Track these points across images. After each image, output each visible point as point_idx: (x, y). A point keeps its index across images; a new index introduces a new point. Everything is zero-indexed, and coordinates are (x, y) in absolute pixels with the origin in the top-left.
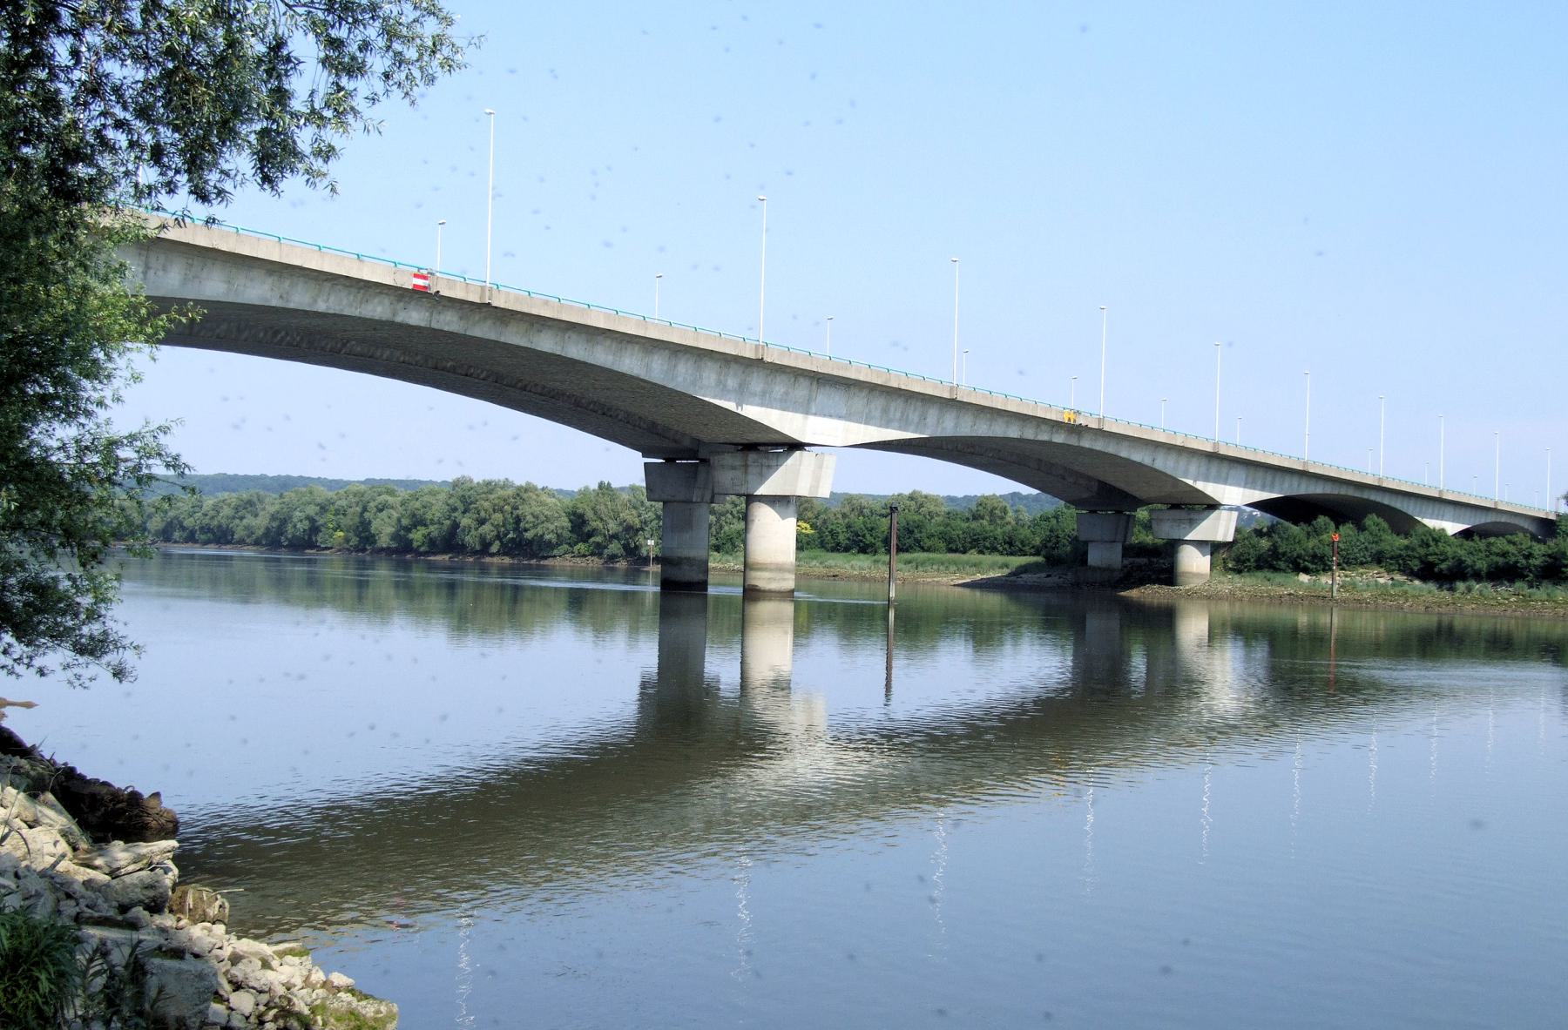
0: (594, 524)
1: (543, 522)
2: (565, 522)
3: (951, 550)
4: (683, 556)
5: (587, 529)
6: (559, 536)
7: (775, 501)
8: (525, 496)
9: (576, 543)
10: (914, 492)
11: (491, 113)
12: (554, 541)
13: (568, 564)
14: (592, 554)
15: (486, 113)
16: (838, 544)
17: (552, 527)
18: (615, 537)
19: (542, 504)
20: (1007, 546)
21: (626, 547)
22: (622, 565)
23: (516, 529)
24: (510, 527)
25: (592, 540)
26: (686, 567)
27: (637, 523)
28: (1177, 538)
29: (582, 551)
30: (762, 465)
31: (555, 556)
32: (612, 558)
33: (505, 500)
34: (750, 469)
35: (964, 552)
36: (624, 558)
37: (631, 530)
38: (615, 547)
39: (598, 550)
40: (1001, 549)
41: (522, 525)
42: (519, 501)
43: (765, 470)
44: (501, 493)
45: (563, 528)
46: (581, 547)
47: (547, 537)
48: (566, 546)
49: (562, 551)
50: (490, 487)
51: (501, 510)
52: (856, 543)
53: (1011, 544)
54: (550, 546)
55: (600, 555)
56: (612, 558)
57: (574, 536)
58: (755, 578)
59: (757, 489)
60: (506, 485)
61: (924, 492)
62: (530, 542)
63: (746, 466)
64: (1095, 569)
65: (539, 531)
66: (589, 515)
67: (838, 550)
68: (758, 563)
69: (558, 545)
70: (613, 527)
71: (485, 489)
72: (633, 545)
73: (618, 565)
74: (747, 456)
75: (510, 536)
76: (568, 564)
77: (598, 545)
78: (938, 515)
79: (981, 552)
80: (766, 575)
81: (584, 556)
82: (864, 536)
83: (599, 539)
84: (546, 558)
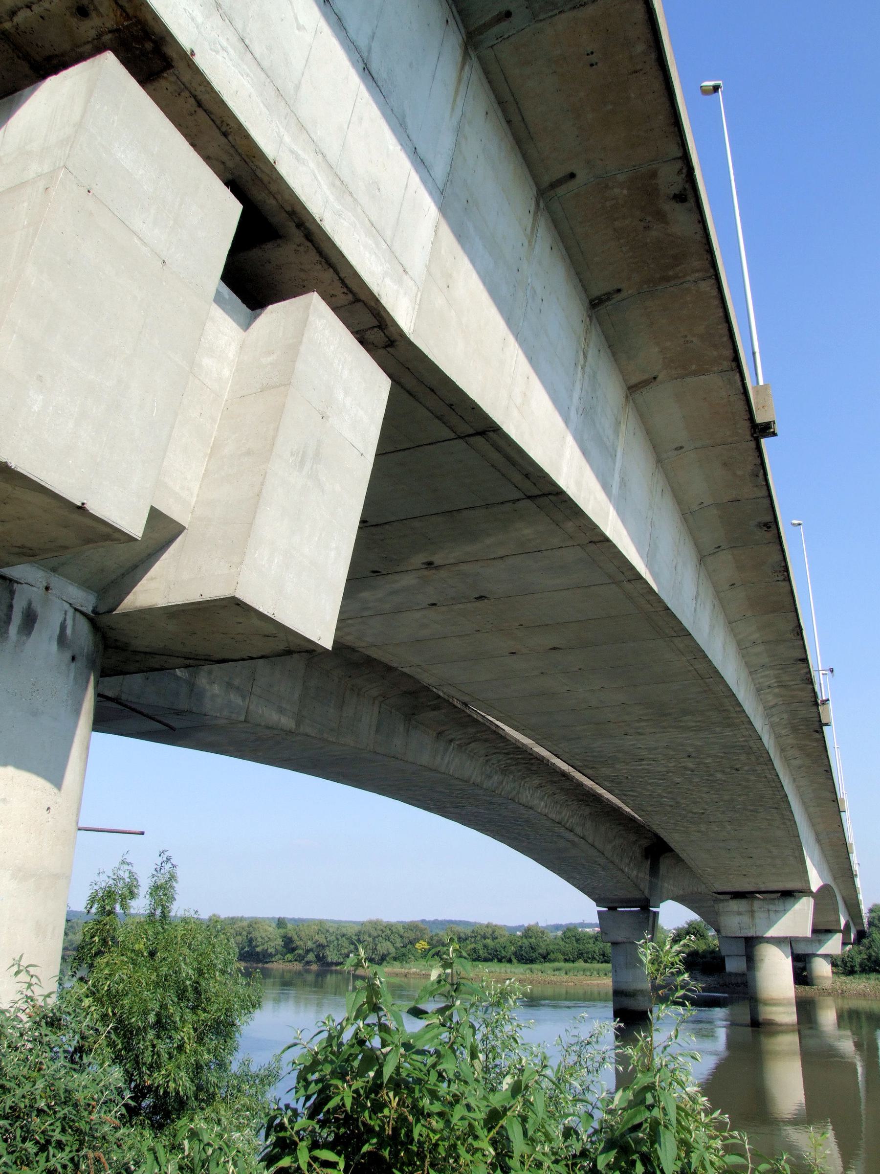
0: (298, 943)
1: (267, 942)
2: (280, 942)
3: (566, 960)
4: (638, 989)
5: (294, 945)
6: (276, 949)
7: (778, 941)
8: (256, 926)
9: (286, 954)
10: (489, 923)
11: (799, 524)
12: (273, 953)
13: (281, 966)
14: (296, 960)
15: (794, 525)
16: (479, 956)
17: (273, 945)
18: (311, 950)
19: (266, 931)
20: (601, 957)
21: (317, 956)
22: (314, 967)
23: (249, 946)
24: (246, 944)
25: (296, 952)
26: (640, 998)
27: (324, 942)
28: (810, 952)
29: (289, 959)
30: (769, 910)
31: (273, 962)
32: (308, 963)
33: (243, 928)
34: (756, 914)
35: (573, 961)
36: (315, 962)
37: (322, 947)
38: (311, 957)
39: (300, 959)
40: (598, 958)
41: (254, 943)
42: (251, 929)
43: (772, 914)
44: (240, 924)
45: (279, 945)
46: (289, 956)
47: (270, 951)
48: (280, 956)
49: (277, 959)
50: (233, 921)
51: (240, 934)
52: (496, 956)
53: (604, 955)
54: (271, 955)
55: (300, 961)
56: (308, 963)
57: (285, 950)
58: (771, 1013)
59: (767, 931)
60: (242, 919)
61: (494, 923)
62: (258, 954)
63: (752, 912)
64: (730, 974)
65: (265, 947)
66: (295, 937)
67: (479, 960)
68: (773, 999)
69: (275, 955)
70: (310, 944)
71: (229, 922)
72: (321, 955)
73: (312, 967)
74: (752, 905)
75: (246, 949)
76: (281, 966)
77: (299, 955)
78: (504, 936)
79: (586, 961)
80: (780, 1009)
81: (291, 961)
82: (500, 952)
83: (300, 952)
84: (267, 963)
